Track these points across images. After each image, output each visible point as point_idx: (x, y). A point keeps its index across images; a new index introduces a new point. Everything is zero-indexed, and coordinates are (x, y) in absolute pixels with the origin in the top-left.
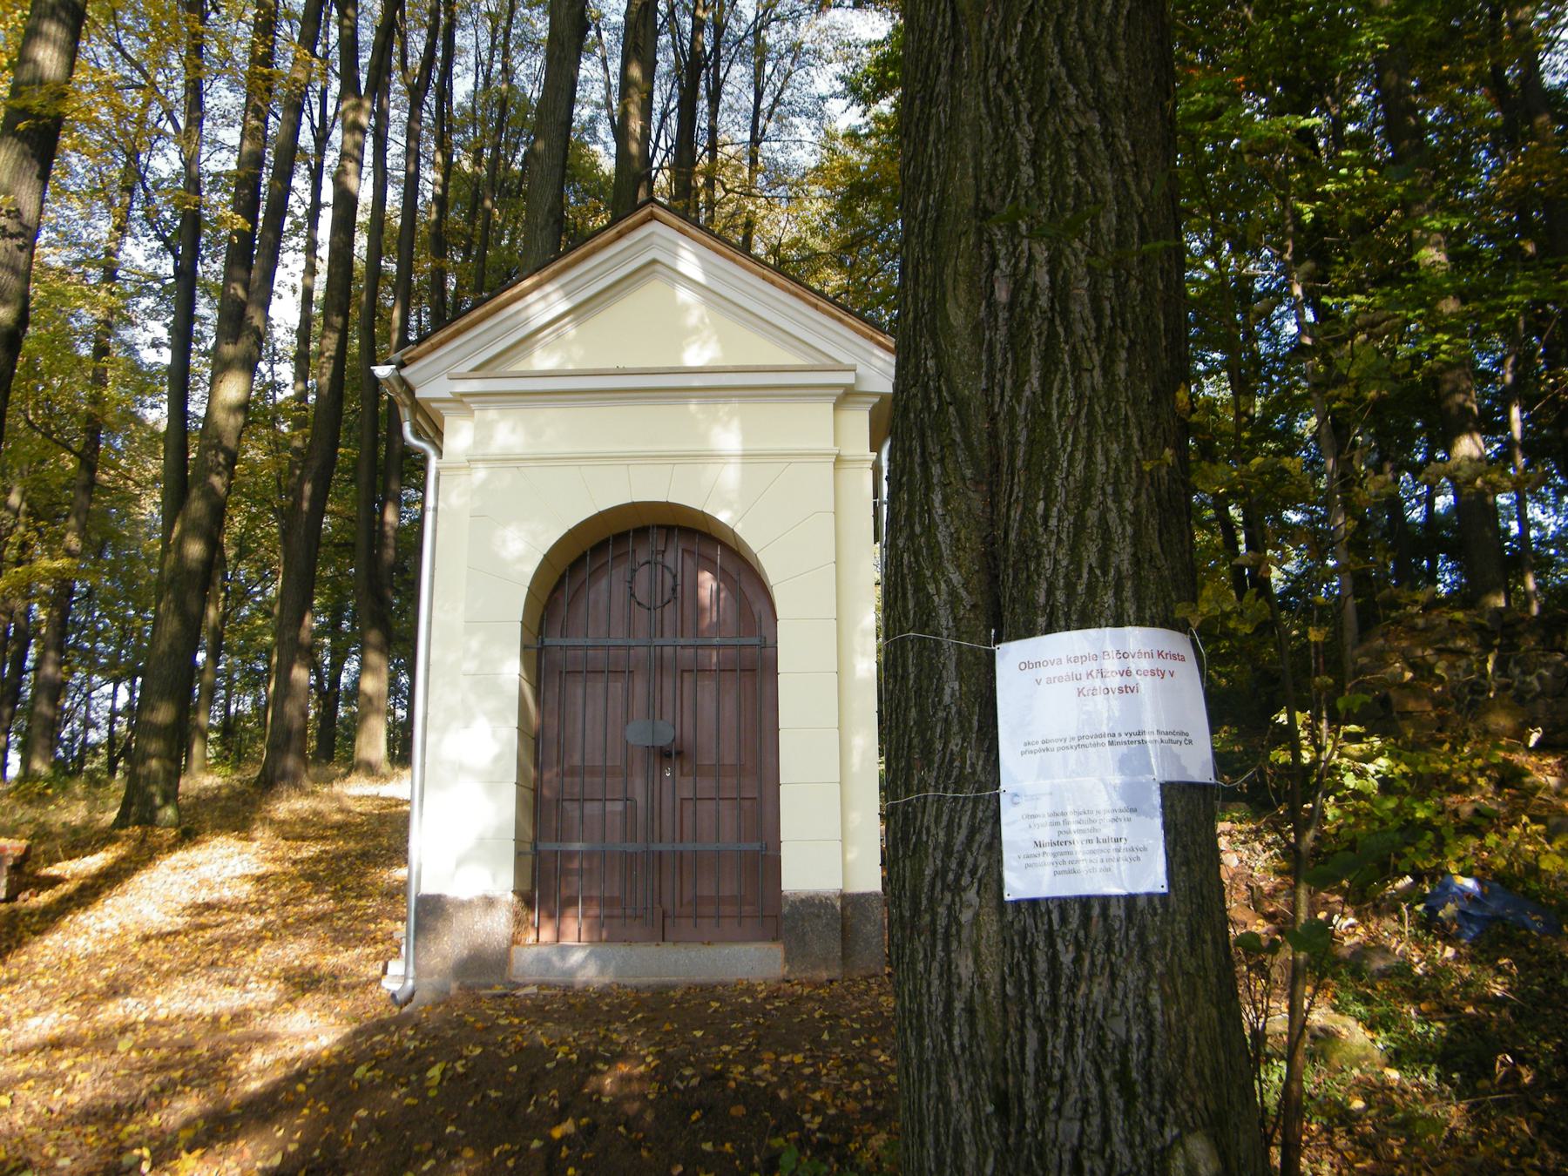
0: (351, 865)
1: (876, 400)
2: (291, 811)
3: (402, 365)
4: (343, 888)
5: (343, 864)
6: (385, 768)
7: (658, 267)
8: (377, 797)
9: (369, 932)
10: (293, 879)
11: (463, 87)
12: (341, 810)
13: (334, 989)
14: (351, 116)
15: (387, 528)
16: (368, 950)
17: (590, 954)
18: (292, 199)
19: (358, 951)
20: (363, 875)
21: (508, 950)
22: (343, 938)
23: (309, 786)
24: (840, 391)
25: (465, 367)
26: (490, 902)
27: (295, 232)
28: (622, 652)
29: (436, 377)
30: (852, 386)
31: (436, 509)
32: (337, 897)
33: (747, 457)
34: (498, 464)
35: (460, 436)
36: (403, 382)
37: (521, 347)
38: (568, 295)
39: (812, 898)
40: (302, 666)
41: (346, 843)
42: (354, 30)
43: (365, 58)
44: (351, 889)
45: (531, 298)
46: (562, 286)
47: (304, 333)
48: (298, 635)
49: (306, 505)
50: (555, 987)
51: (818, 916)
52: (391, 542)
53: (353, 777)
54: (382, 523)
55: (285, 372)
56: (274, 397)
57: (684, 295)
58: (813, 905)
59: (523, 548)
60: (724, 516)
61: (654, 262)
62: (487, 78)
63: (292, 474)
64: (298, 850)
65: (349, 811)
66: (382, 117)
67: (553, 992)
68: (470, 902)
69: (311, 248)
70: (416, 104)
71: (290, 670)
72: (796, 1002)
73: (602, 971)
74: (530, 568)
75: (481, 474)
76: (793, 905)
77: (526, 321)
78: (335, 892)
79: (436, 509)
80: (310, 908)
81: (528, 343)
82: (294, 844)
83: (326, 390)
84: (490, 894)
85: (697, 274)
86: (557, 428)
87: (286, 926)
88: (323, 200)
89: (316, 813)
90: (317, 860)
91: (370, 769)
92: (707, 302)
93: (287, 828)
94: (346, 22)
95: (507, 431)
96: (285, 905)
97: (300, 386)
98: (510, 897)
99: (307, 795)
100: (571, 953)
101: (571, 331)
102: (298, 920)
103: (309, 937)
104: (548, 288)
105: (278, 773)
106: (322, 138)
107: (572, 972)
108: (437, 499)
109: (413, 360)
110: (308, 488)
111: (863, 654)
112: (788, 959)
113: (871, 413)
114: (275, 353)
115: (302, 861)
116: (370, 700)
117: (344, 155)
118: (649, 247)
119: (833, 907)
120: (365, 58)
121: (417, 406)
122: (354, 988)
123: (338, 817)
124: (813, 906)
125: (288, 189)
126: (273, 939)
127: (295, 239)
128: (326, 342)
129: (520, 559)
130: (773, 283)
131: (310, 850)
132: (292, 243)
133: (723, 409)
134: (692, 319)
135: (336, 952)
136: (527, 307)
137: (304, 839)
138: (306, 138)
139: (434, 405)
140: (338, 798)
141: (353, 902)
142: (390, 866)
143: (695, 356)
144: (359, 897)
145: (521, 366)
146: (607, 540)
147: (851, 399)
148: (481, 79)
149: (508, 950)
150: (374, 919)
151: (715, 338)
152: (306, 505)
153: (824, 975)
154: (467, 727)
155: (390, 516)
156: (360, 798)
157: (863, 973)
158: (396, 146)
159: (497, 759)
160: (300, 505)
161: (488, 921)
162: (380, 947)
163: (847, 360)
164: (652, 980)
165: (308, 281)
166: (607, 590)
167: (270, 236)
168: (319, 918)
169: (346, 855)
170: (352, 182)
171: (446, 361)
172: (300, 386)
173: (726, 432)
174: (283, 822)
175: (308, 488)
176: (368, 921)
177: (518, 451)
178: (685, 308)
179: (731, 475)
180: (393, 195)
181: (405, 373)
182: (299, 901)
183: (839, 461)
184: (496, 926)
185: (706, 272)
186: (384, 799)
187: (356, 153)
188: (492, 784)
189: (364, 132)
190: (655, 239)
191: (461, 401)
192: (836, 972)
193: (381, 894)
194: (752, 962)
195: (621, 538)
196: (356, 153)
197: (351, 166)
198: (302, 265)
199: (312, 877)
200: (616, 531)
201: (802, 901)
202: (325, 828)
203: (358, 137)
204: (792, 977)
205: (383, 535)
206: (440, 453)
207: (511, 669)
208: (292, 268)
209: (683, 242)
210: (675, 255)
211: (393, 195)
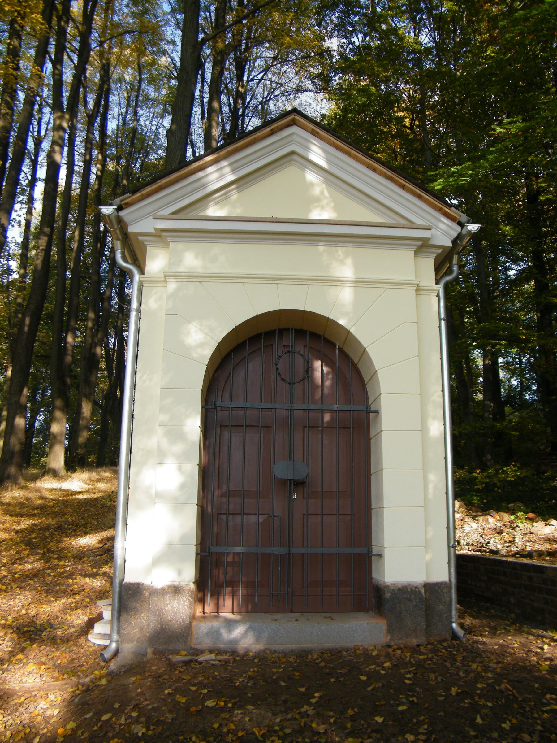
0: (52, 535)
1: (439, 251)
2: (13, 498)
3: (120, 208)
4: (49, 551)
5: (47, 534)
6: (63, 472)
7: (295, 157)
8: (60, 490)
9: (69, 585)
10: (16, 544)
11: (112, 125)
12: (41, 498)
13: (53, 641)
14: (58, 122)
15: (68, 345)
16: (70, 600)
17: (250, 628)
18: (22, 175)
19: (63, 601)
20: (60, 542)
21: (190, 624)
22: (53, 590)
23: (22, 482)
24: (420, 243)
25: (167, 212)
26: (176, 590)
27: (23, 192)
28: (242, 413)
29: (143, 218)
30: (429, 239)
31: (138, 311)
32: (46, 558)
33: (358, 283)
34: (185, 279)
35: (156, 262)
36: (120, 220)
37: (198, 205)
38: (234, 171)
39: (406, 587)
40: (20, 417)
41: (47, 519)
42: (61, 74)
43: (66, 95)
44: (53, 552)
45: (210, 170)
46: (230, 164)
47: (25, 245)
48: (19, 400)
49: (26, 329)
50: (225, 652)
51: (410, 600)
52: (70, 352)
53: (46, 477)
54: (66, 343)
55: (14, 265)
56: (8, 278)
57: (311, 176)
58: (407, 592)
59: (202, 340)
60: (342, 322)
61: (293, 153)
62: (124, 121)
63: (16, 316)
64: (18, 523)
65: (46, 498)
66: (73, 128)
67: (225, 657)
68: (163, 589)
69: (31, 200)
70: (90, 131)
71: (14, 419)
72: (400, 664)
73: (258, 640)
74: (208, 352)
75: (172, 286)
76: (393, 592)
77: (204, 186)
78: (44, 554)
79: (138, 311)
80: (28, 566)
81: (204, 202)
82: (16, 519)
83: (39, 267)
84: (176, 583)
85: (322, 162)
86: (222, 257)
87: (14, 580)
88: (38, 176)
89: (27, 499)
90: (31, 530)
91: (55, 474)
92: (327, 182)
93: (11, 508)
94: (57, 72)
95: (191, 258)
96: (13, 563)
97: (22, 271)
98: (192, 586)
99: (22, 488)
100: (233, 629)
101: (234, 196)
102: (22, 575)
103: (31, 590)
104: (224, 163)
105: (6, 475)
106: (38, 143)
107: (235, 642)
108: (140, 304)
109: (128, 205)
110: (27, 320)
111: (434, 418)
112: (390, 630)
113: (435, 260)
114: (9, 255)
115: (21, 531)
116: (55, 436)
117: (54, 143)
118: (290, 143)
119: (420, 593)
120: (66, 95)
121: (126, 238)
122: (68, 641)
123: (39, 502)
124: (406, 593)
125: (20, 171)
126: (6, 591)
127: (22, 197)
128: (40, 241)
129: (202, 345)
130: (374, 170)
131: (25, 523)
132: (20, 199)
133: (340, 251)
134: (317, 191)
135: (50, 602)
136: (207, 176)
137: (21, 515)
138: (31, 144)
139: (140, 238)
140: (38, 490)
141: (56, 562)
142: (76, 536)
143: (316, 215)
144: (60, 558)
145: (202, 214)
146: (261, 334)
147: (424, 249)
148: (121, 121)
149: (190, 624)
150: (71, 575)
151: (332, 204)
152: (26, 329)
153: (415, 642)
154: (161, 463)
155: (70, 339)
156: (52, 490)
157: (437, 638)
158: (80, 148)
159: (183, 487)
160: (23, 328)
161: (175, 604)
162: (77, 597)
163: (419, 222)
164: (295, 646)
165: (29, 217)
166: (253, 368)
167: (13, 173)
168: (36, 575)
169: (48, 528)
170: (57, 157)
171: (150, 209)
172: (22, 271)
173: (344, 266)
174: (9, 504)
175: (27, 320)
176: (67, 577)
177: (200, 270)
178: (312, 185)
179: (346, 295)
180: (76, 179)
181: (122, 213)
182: (22, 560)
183: (418, 289)
184: (179, 609)
185: (328, 161)
186: (64, 491)
187: (60, 142)
188: (177, 505)
189: (64, 130)
190: (295, 137)
191: (161, 236)
192: (422, 640)
193: (74, 557)
194: (363, 631)
195: (270, 334)
196: (60, 142)
197: (57, 148)
198: (25, 211)
199: (28, 543)
200: (281, 327)
201: (399, 589)
202: (34, 509)
203: (61, 133)
204: (392, 643)
205: (65, 348)
206: (142, 272)
207: (193, 425)
208: (19, 212)
209: (314, 140)
210: (308, 149)
211: (76, 179)
